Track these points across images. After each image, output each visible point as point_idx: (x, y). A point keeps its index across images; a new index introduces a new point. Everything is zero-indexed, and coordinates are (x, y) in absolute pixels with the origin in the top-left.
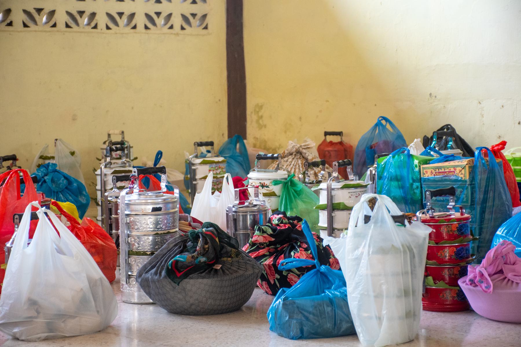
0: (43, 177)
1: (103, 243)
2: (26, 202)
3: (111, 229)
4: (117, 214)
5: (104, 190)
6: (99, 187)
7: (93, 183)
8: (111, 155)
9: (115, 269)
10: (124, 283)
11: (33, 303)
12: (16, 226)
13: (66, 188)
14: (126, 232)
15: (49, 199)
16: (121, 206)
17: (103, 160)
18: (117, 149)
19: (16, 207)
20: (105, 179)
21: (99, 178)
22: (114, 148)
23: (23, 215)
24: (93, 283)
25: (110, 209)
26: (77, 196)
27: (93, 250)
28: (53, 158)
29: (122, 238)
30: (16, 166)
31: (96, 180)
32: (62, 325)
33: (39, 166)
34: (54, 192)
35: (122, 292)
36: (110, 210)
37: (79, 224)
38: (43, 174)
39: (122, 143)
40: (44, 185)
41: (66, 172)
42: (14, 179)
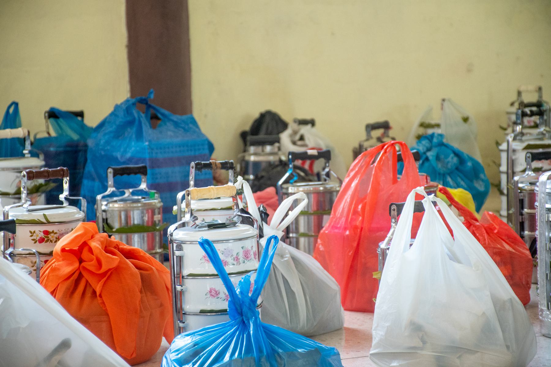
0: (425, 153)
1: (511, 249)
2: (404, 187)
3: (522, 229)
4: (532, 207)
5: (511, 173)
6: (504, 168)
7: (494, 162)
8: (522, 123)
9: (529, 288)
10: (545, 308)
11: (416, 328)
12: (393, 220)
13: (457, 169)
14: (547, 234)
15: (435, 184)
16: (540, 197)
17: (510, 130)
18: (532, 114)
19: (392, 194)
20: (514, 157)
21: (504, 156)
22: (529, 112)
23: (403, 205)
24: (499, 306)
25: (523, 201)
26: (471, 181)
27: (498, 258)
28: (438, 126)
29: (541, 242)
30: (388, 136)
31: (500, 158)
32: (458, 361)
33: (419, 138)
34: (439, 174)
35: (541, 321)
36: (522, 202)
37: (476, 220)
38: (425, 149)
39: (539, 105)
40: (426, 164)
41: (456, 145)
42: (390, 155)
